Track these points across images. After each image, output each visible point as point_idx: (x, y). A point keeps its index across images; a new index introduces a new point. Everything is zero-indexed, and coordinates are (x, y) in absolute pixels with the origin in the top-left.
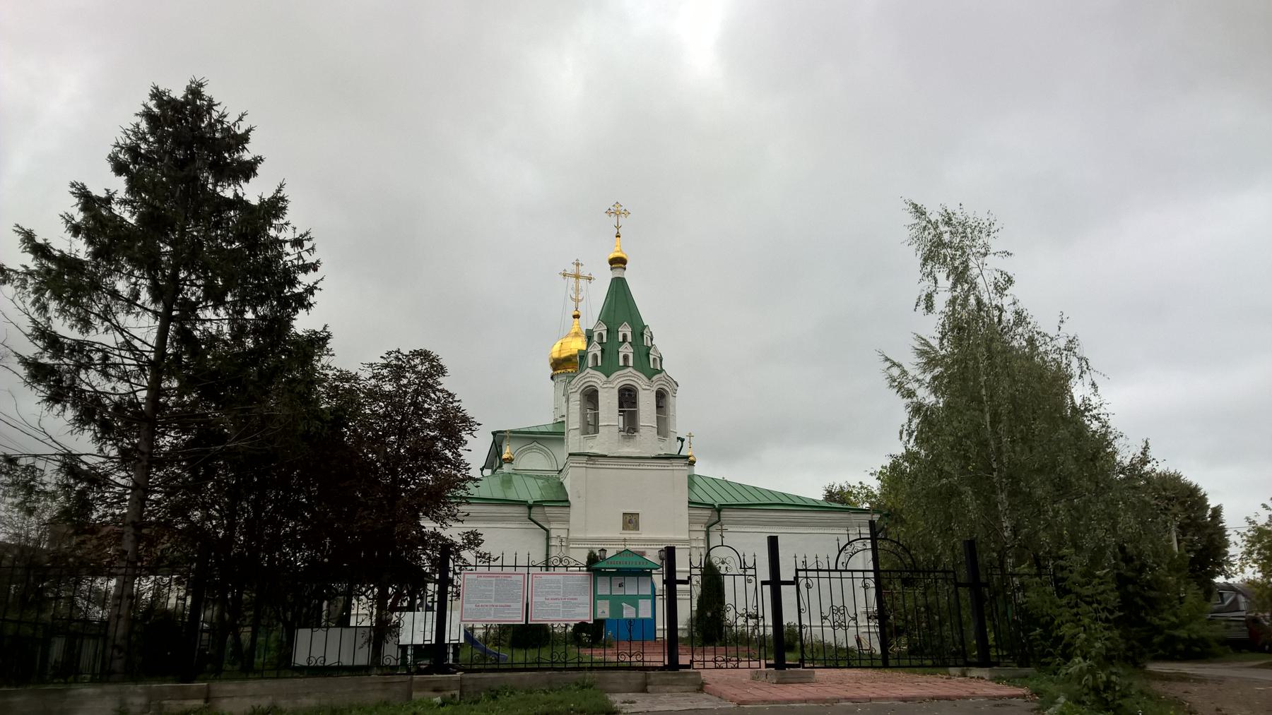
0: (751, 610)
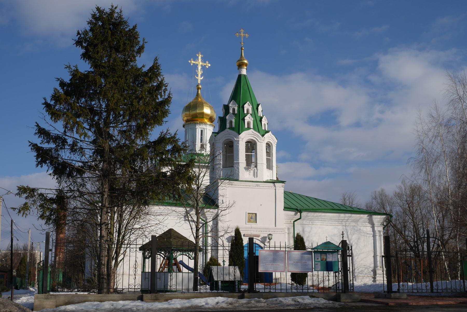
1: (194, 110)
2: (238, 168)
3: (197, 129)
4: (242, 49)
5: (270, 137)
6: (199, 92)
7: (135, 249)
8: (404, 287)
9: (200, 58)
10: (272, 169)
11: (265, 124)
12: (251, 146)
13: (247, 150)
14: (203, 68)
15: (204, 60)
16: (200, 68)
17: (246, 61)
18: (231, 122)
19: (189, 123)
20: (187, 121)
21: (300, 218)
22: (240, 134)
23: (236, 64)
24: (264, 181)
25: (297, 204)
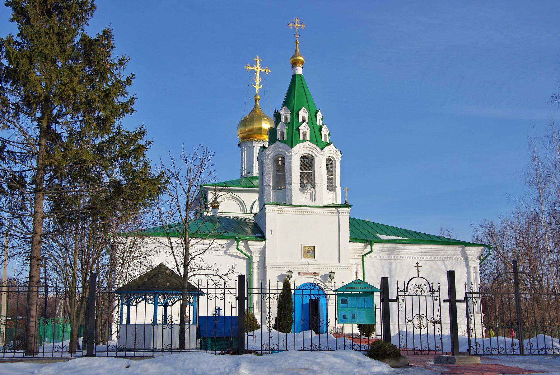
0: (437, 319)
1: (251, 125)
2: (291, 190)
3: (255, 148)
4: (297, 43)
5: (331, 151)
6: (258, 104)
7: (214, 295)
8: (478, 346)
9: (258, 62)
10: (335, 191)
11: (325, 135)
12: (307, 163)
13: (302, 167)
14: (262, 74)
15: (262, 65)
16: (258, 74)
17: (301, 58)
18: (282, 133)
19: (245, 140)
20: (243, 138)
21: (371, 252)
22: (292, 148)
23: (290, 61)
24: (325, 205)
25: (364, 232)
